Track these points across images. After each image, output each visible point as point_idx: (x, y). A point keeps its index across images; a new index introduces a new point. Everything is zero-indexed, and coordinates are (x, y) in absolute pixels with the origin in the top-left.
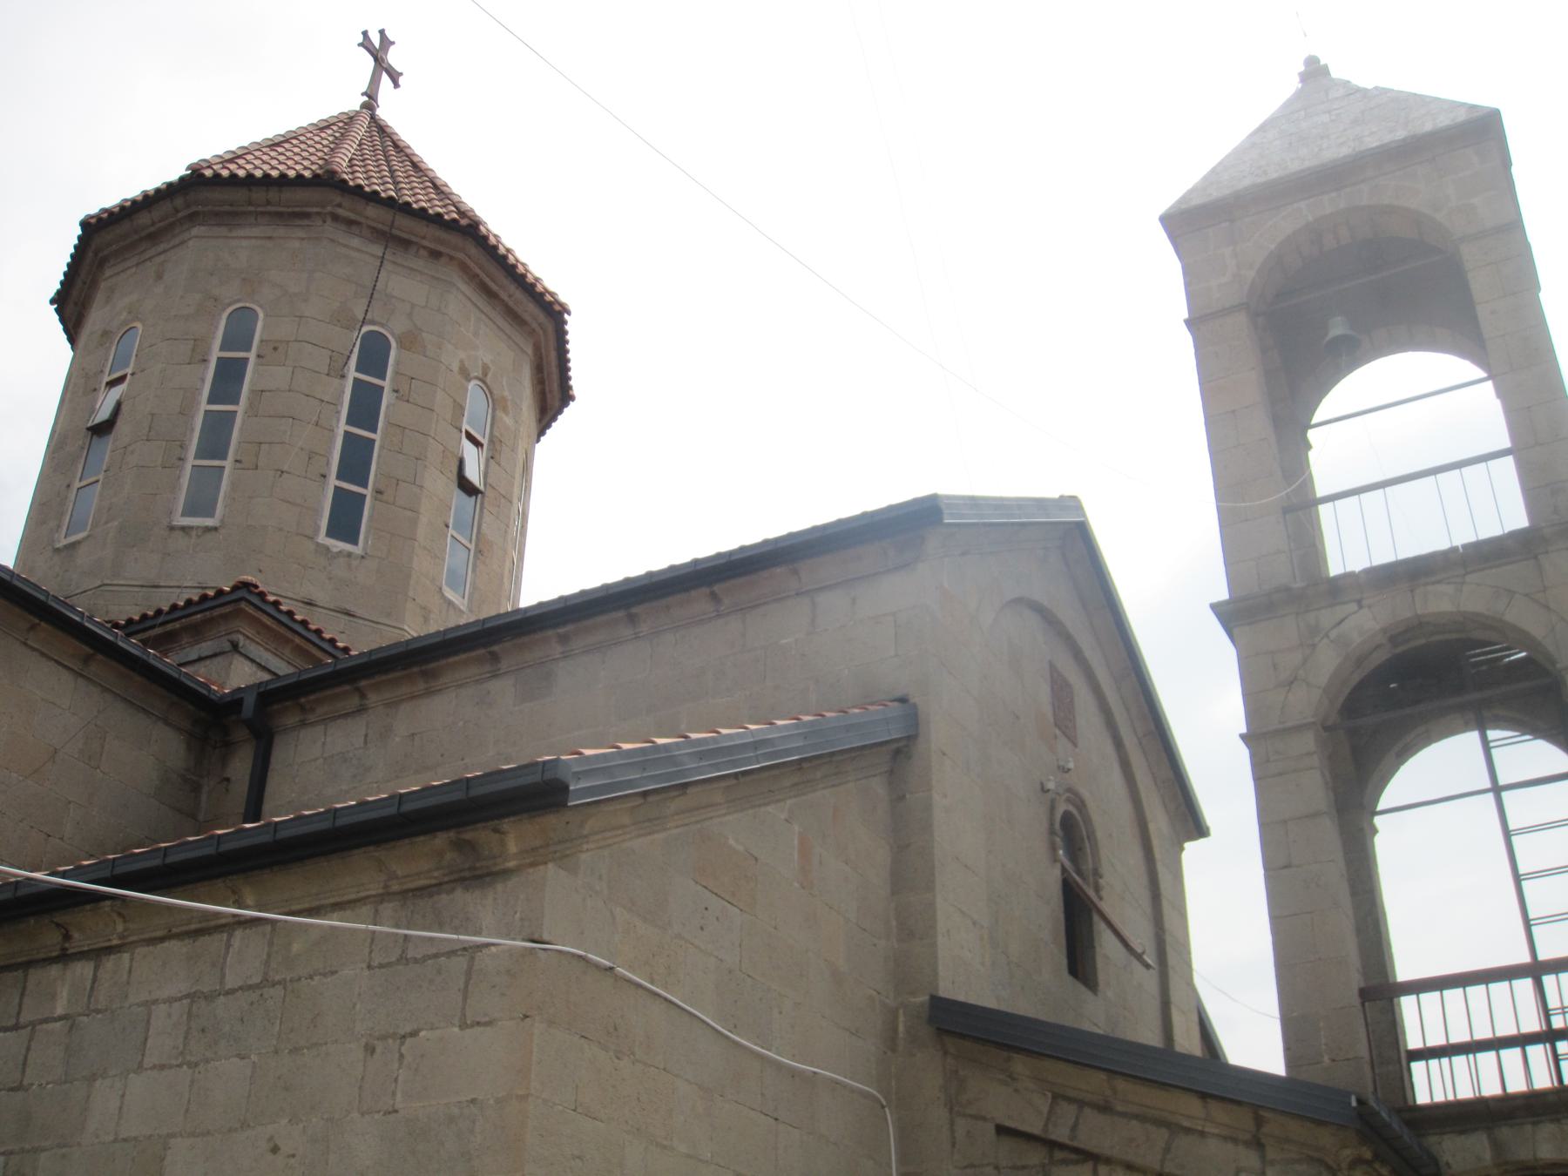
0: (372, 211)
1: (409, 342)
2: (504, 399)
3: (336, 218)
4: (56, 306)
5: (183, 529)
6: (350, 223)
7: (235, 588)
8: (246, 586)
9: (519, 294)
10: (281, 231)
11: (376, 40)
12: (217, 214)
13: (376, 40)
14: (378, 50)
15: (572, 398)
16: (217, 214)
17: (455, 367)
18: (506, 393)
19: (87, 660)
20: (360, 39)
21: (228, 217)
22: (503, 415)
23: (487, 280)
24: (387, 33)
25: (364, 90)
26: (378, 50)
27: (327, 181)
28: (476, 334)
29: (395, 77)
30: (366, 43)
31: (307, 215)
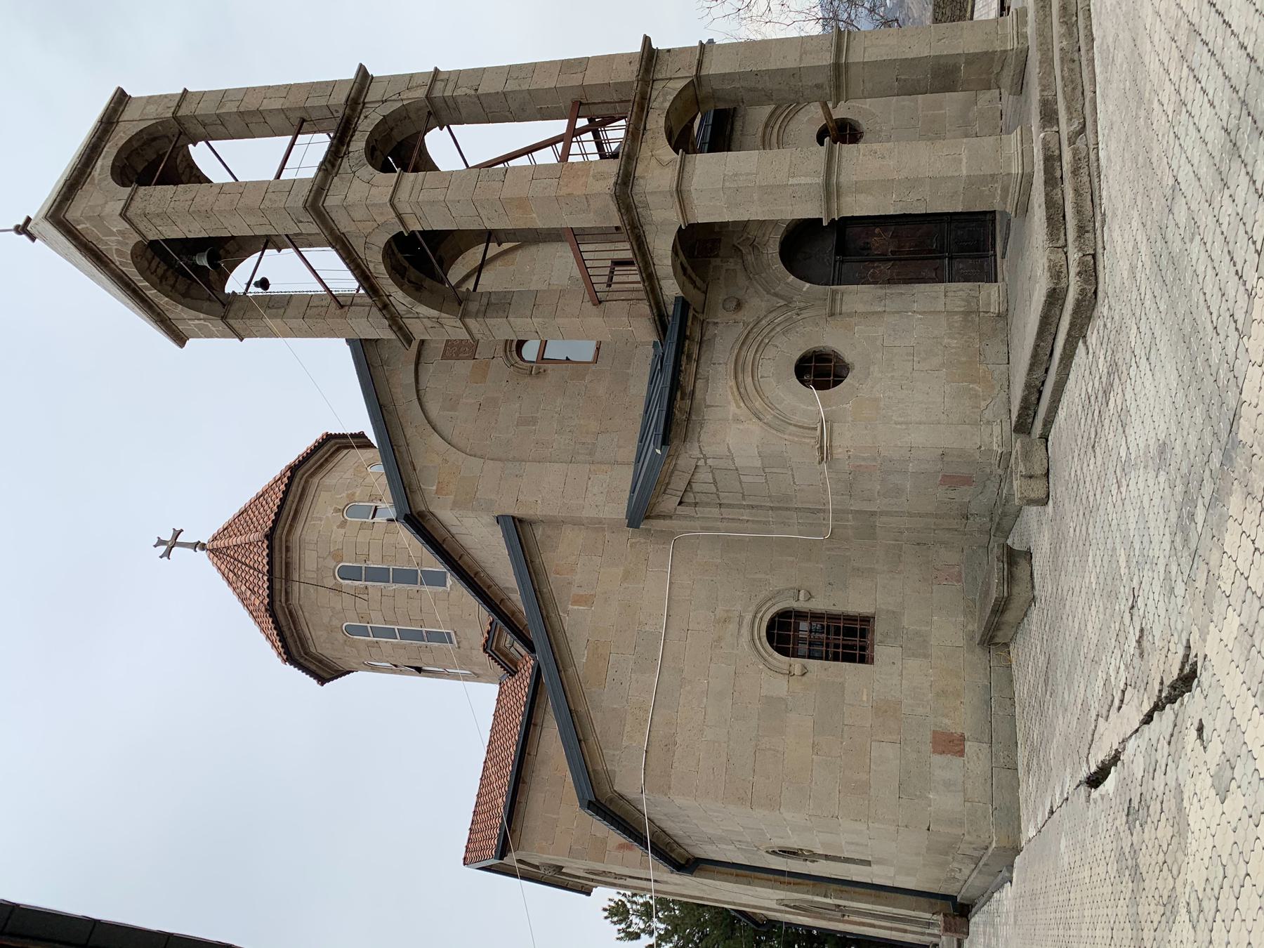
0: (277, 586)
1: (338, 556)
2: (348, 496)
3: (287, 600)
4: (191, 146)
5: (458, 643)
6: (287, 593)
7: (487, 653)
8: (485, 650)
9: (290, 498)
10: (302, 620)
11: (163, 548)
12: (302, 645)
13: (163, 548)
14: (170, 545)
15: (327, 435)
16: (302, 645)
17: (342, 531)
18: (344, 495)
19: (535, 725)
20: (165, 558)
21: (302, 641)
22: (357, 494)
23: (290, 518)
24: (155, 543)
25: (192, 551)
26: (170, 545)
27: (271, 610)
28: (320, 519)
29: (177, 533)
30: (167, 554)
31: (290, 612)
